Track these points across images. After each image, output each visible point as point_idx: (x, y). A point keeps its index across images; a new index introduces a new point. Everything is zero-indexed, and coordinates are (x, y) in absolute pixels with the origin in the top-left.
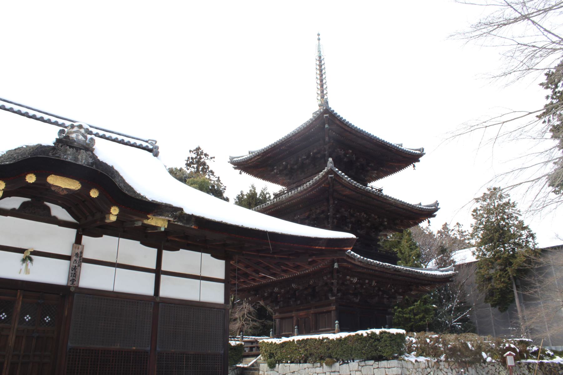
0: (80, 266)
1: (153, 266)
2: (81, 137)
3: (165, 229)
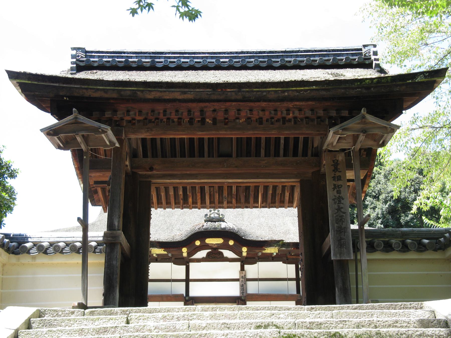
0: (245, 284)
1: (184, 277)
2: (216, 215)
3: (277, 253)
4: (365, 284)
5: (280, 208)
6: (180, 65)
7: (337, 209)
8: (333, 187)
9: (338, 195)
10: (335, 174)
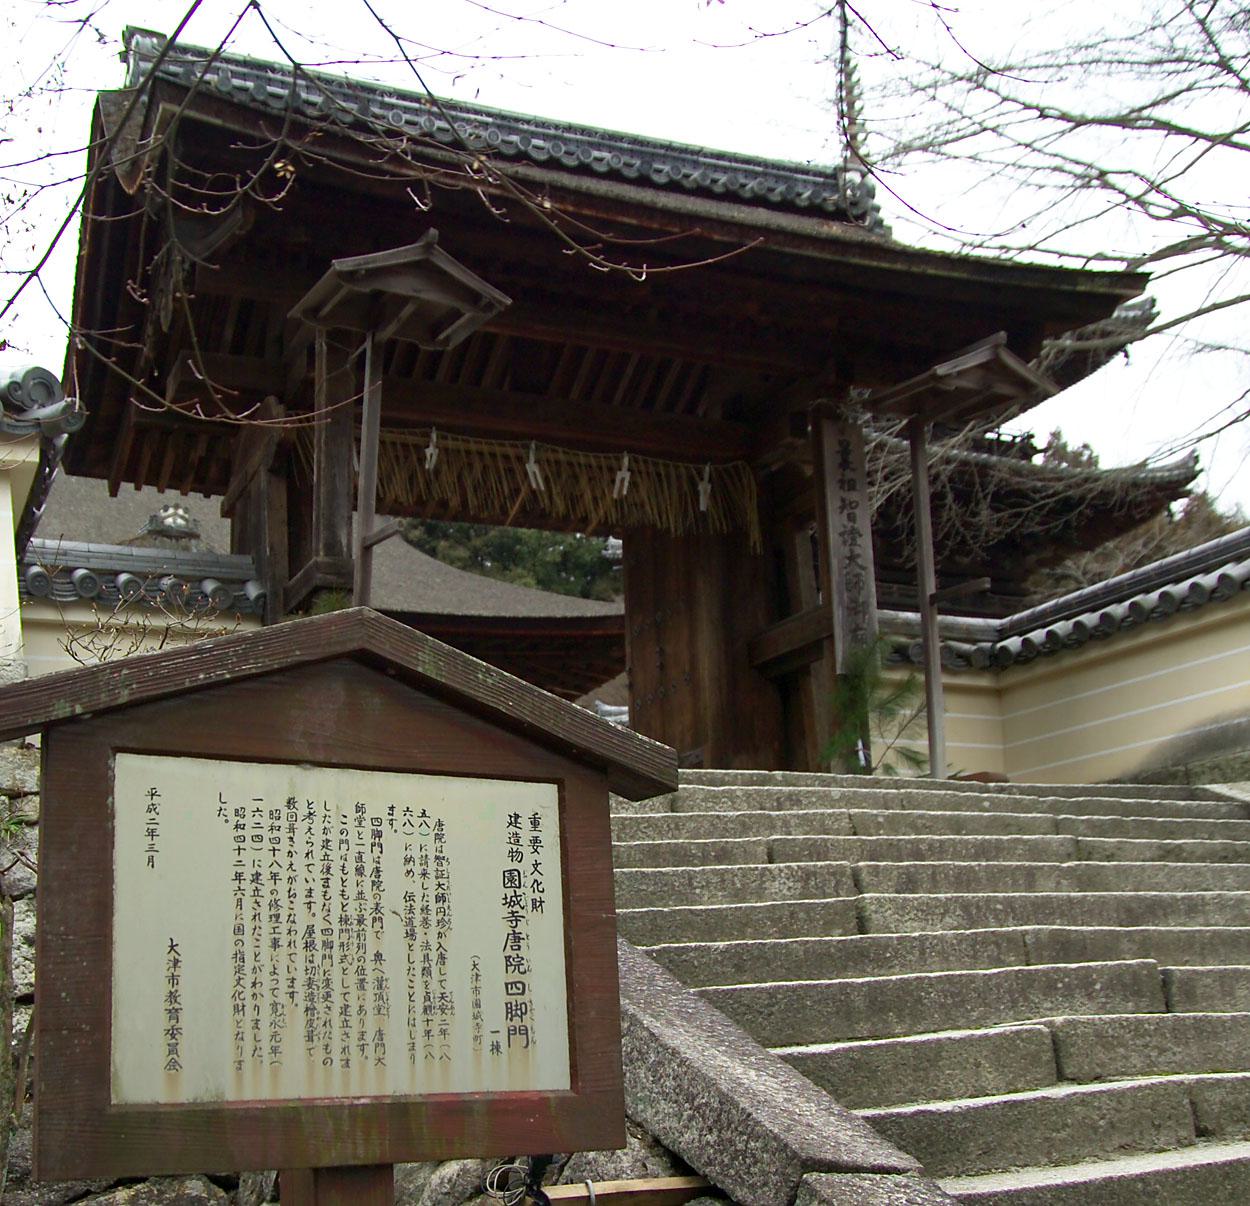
9: (851, 524)
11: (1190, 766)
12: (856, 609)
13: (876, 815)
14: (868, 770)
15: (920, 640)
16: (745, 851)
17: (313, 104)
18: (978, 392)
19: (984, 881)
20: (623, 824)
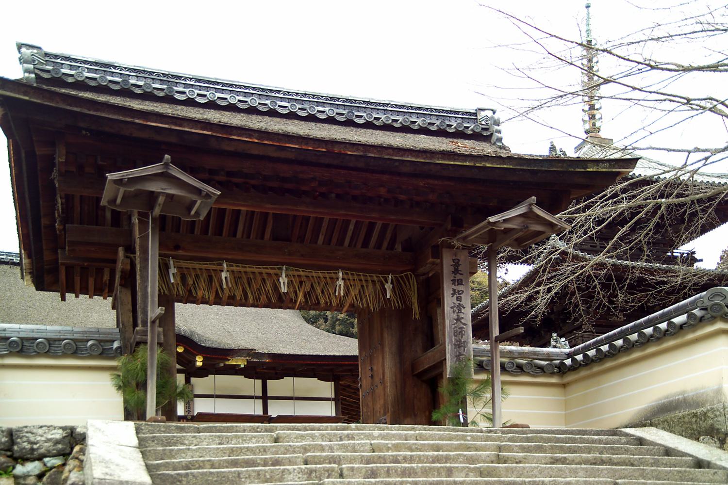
0: (192, 400)
1: (259, 393)
4: (363, 409)
5: (201, 305)
6: (214, 101)
7: (455, 320)
8: (452, 292)
9: (459, 302)
10: (455, 277)
11: (653, 421)
12: (460, 345)
13: (387, 444)
14: (465, 424)
15: (490, 358)
16: (290, 461)
17: (139, 86)
18: (521, 230)
19: (420, 473)
20: (232, 450)
